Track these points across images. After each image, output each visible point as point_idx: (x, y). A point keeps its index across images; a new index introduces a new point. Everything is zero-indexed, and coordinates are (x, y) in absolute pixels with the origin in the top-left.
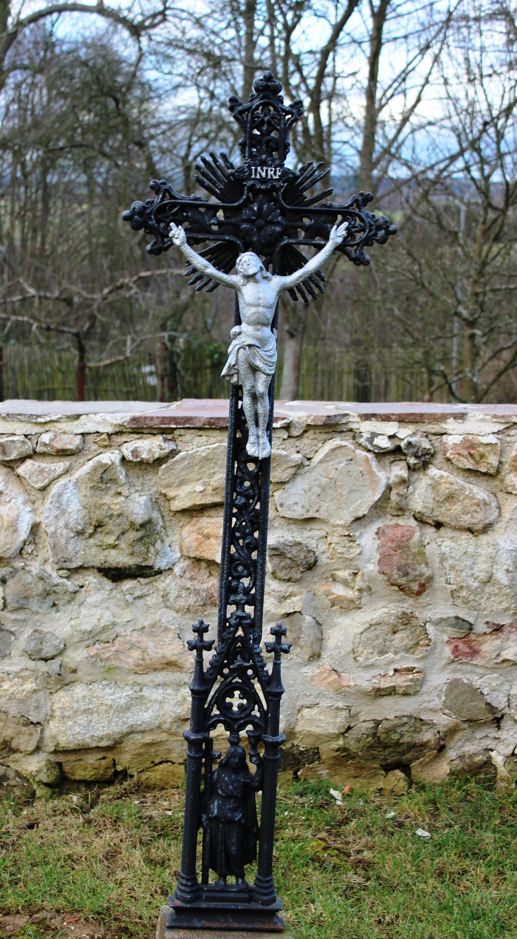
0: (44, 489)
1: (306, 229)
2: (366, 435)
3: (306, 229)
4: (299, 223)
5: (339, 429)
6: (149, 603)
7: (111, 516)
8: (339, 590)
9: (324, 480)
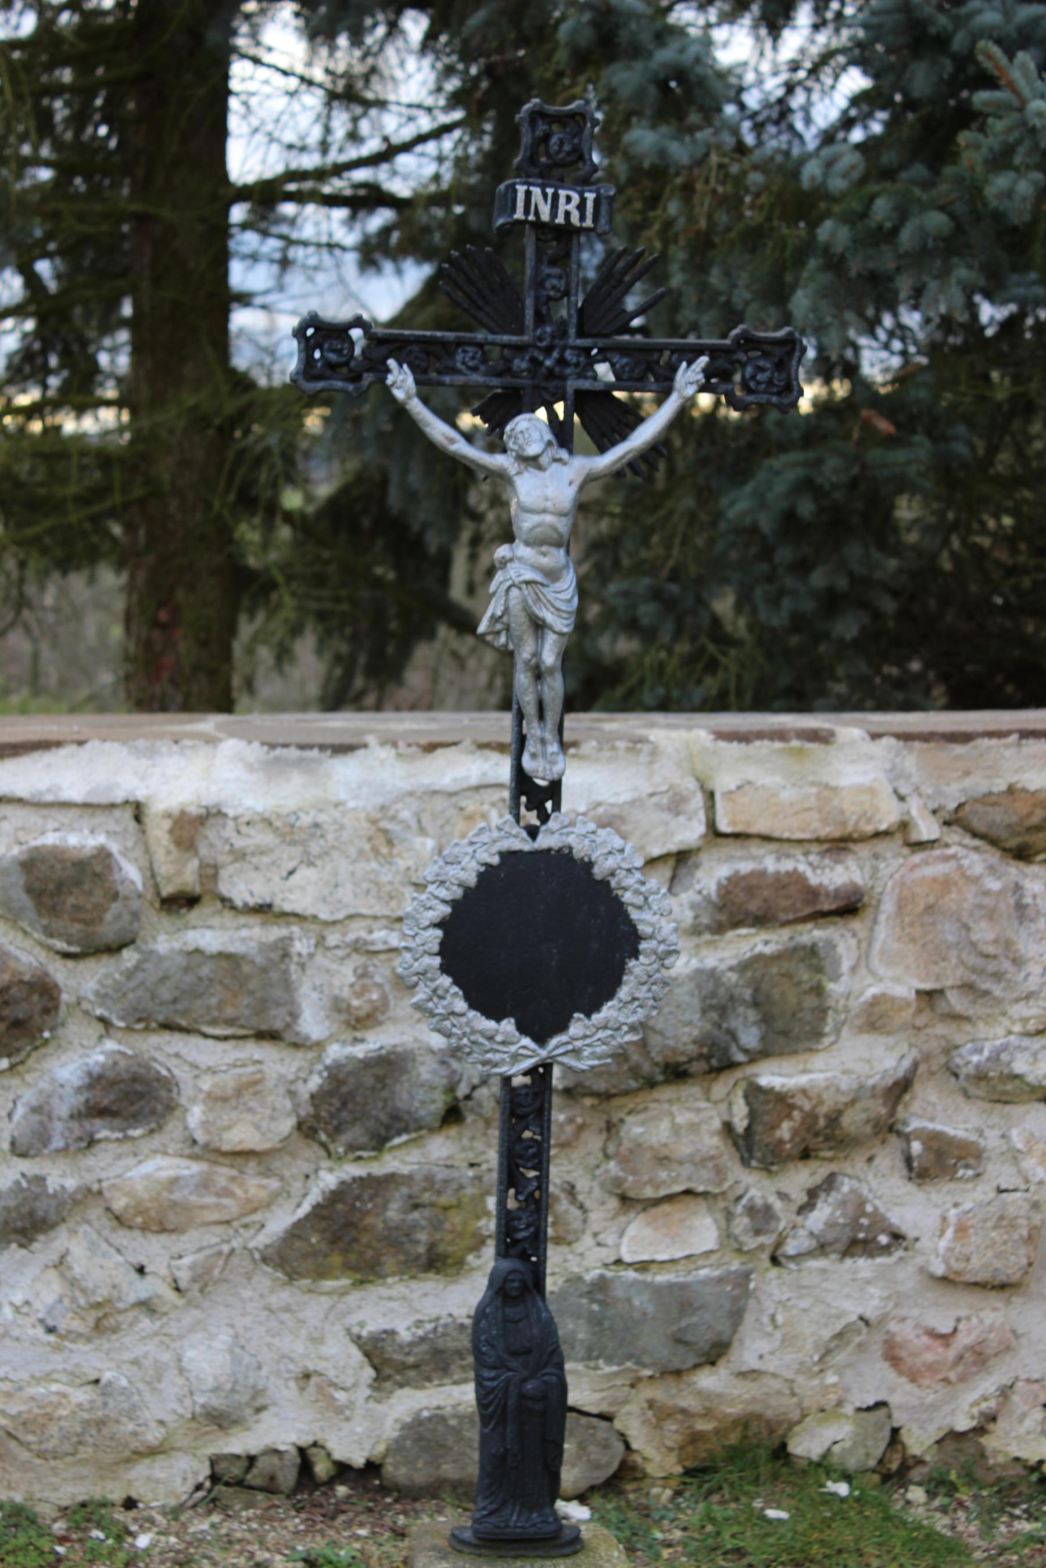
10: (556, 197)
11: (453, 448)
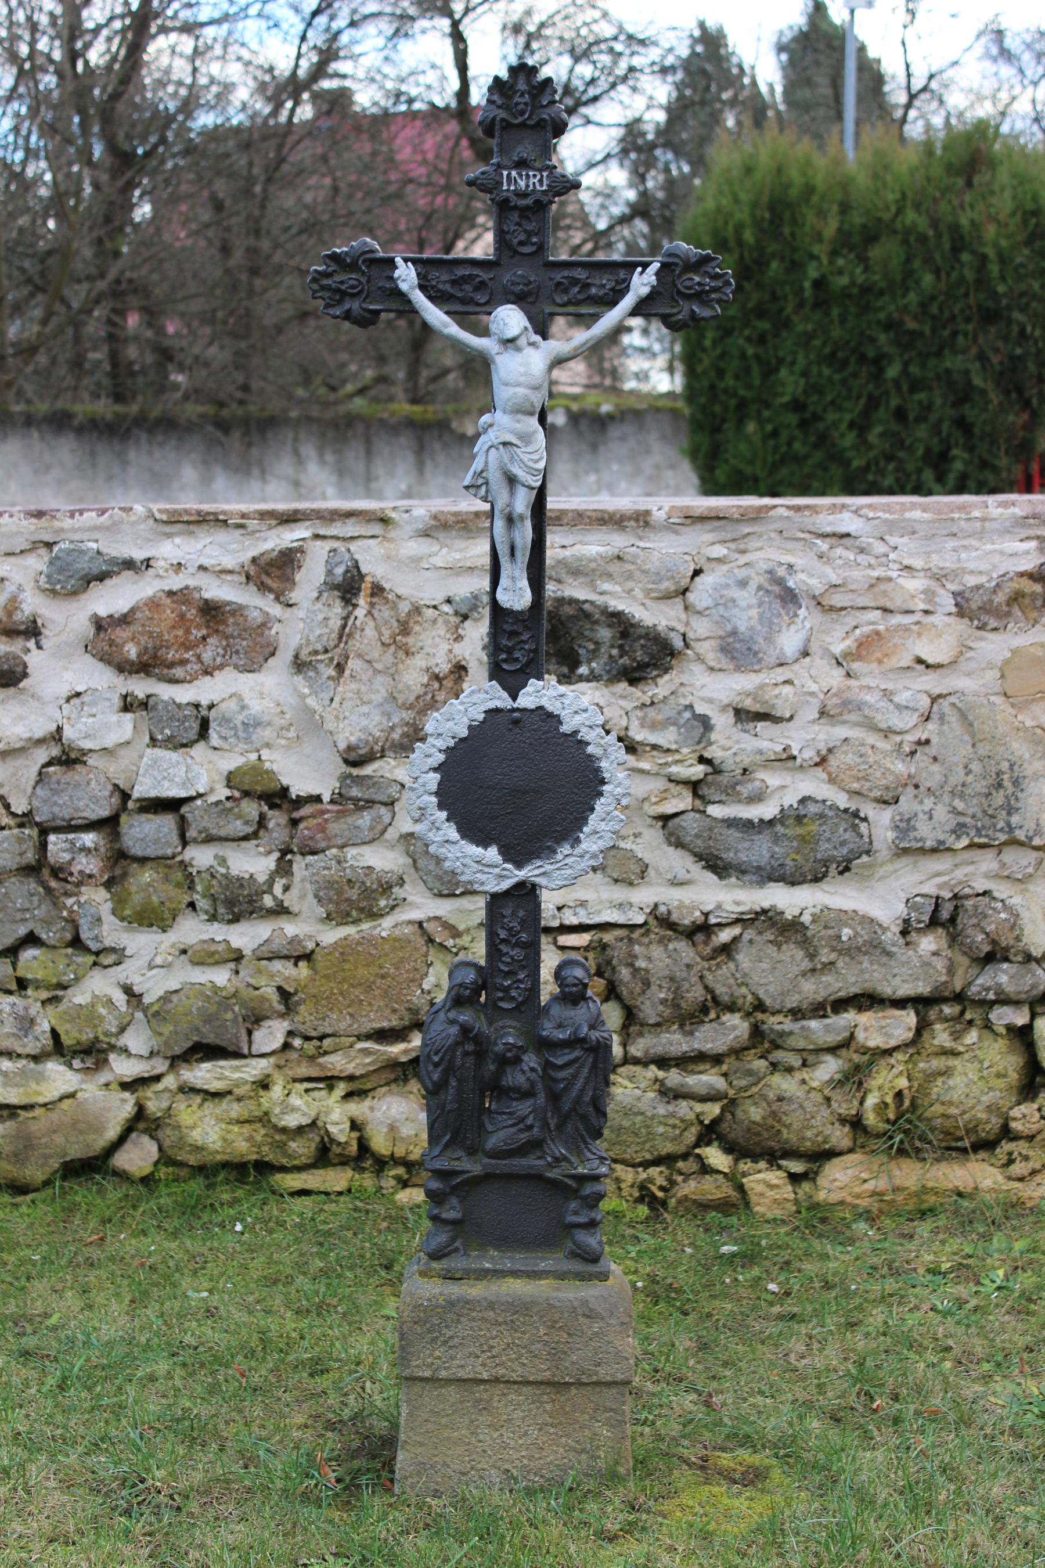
11: (446, 331)
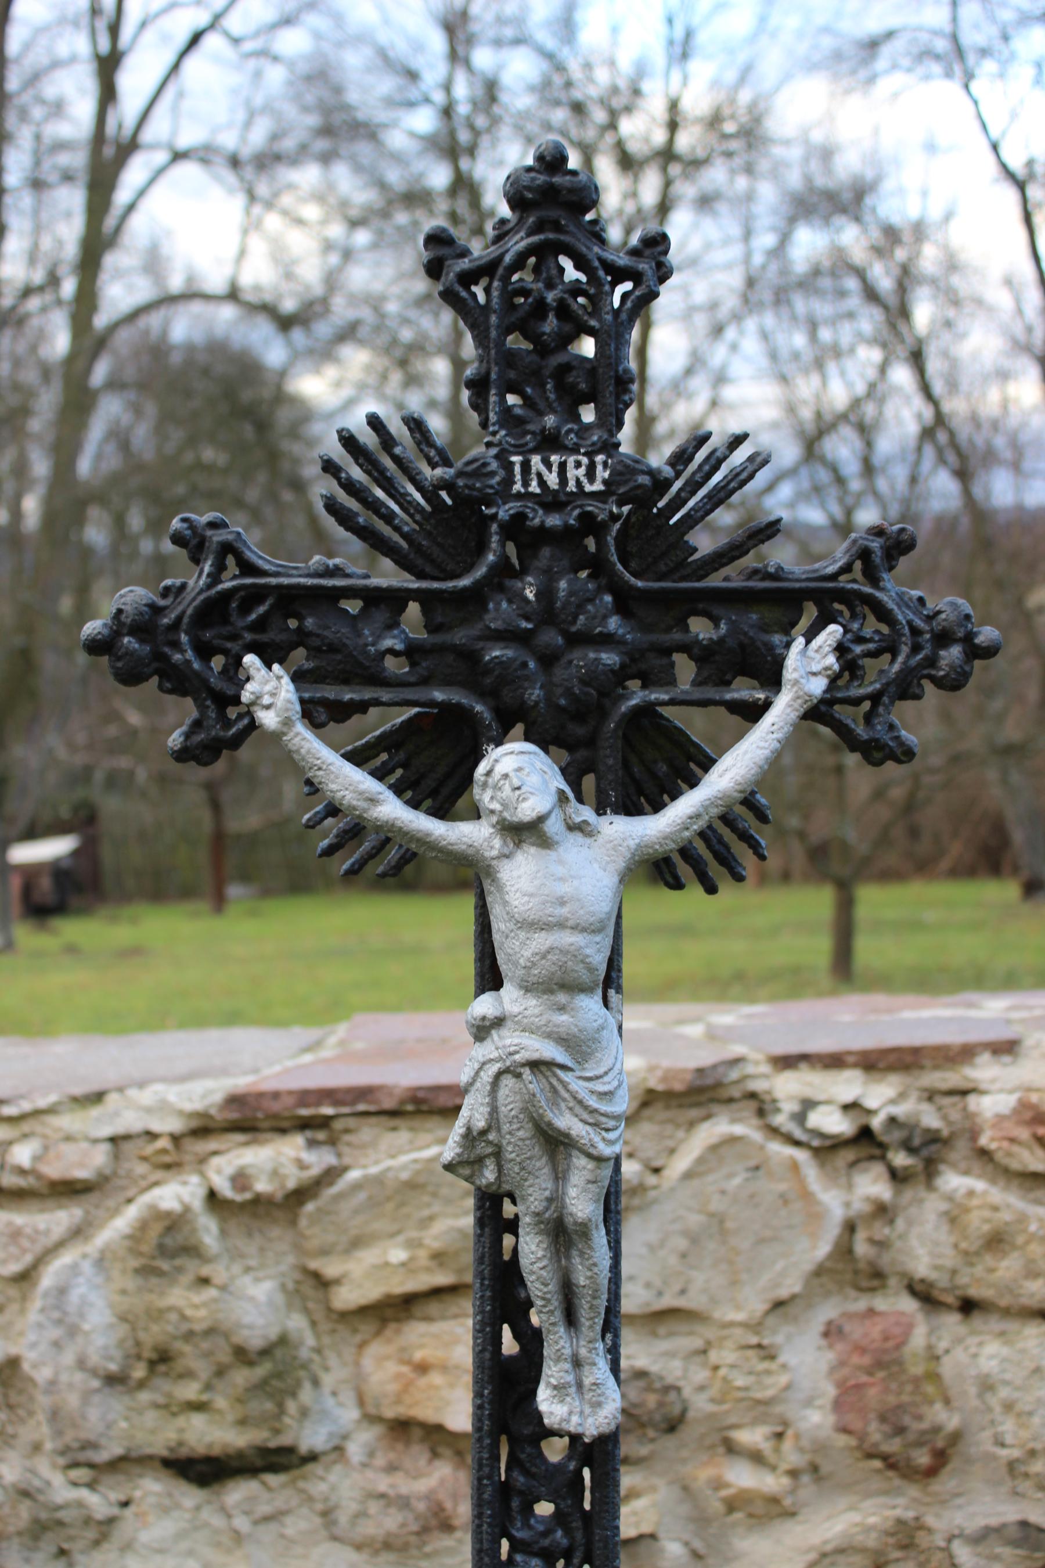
0: (25, 1278)
1: (703, 655)
2: (789, 1107)
3: (703, 655)
4: (677, 636)
5: (725, 1093)
6: (289, 1531)
7: (189, 1336)
8: (743, 1477)
9: (695, 1220)
10: (563, 466)
